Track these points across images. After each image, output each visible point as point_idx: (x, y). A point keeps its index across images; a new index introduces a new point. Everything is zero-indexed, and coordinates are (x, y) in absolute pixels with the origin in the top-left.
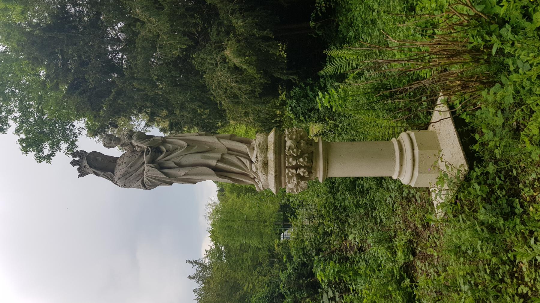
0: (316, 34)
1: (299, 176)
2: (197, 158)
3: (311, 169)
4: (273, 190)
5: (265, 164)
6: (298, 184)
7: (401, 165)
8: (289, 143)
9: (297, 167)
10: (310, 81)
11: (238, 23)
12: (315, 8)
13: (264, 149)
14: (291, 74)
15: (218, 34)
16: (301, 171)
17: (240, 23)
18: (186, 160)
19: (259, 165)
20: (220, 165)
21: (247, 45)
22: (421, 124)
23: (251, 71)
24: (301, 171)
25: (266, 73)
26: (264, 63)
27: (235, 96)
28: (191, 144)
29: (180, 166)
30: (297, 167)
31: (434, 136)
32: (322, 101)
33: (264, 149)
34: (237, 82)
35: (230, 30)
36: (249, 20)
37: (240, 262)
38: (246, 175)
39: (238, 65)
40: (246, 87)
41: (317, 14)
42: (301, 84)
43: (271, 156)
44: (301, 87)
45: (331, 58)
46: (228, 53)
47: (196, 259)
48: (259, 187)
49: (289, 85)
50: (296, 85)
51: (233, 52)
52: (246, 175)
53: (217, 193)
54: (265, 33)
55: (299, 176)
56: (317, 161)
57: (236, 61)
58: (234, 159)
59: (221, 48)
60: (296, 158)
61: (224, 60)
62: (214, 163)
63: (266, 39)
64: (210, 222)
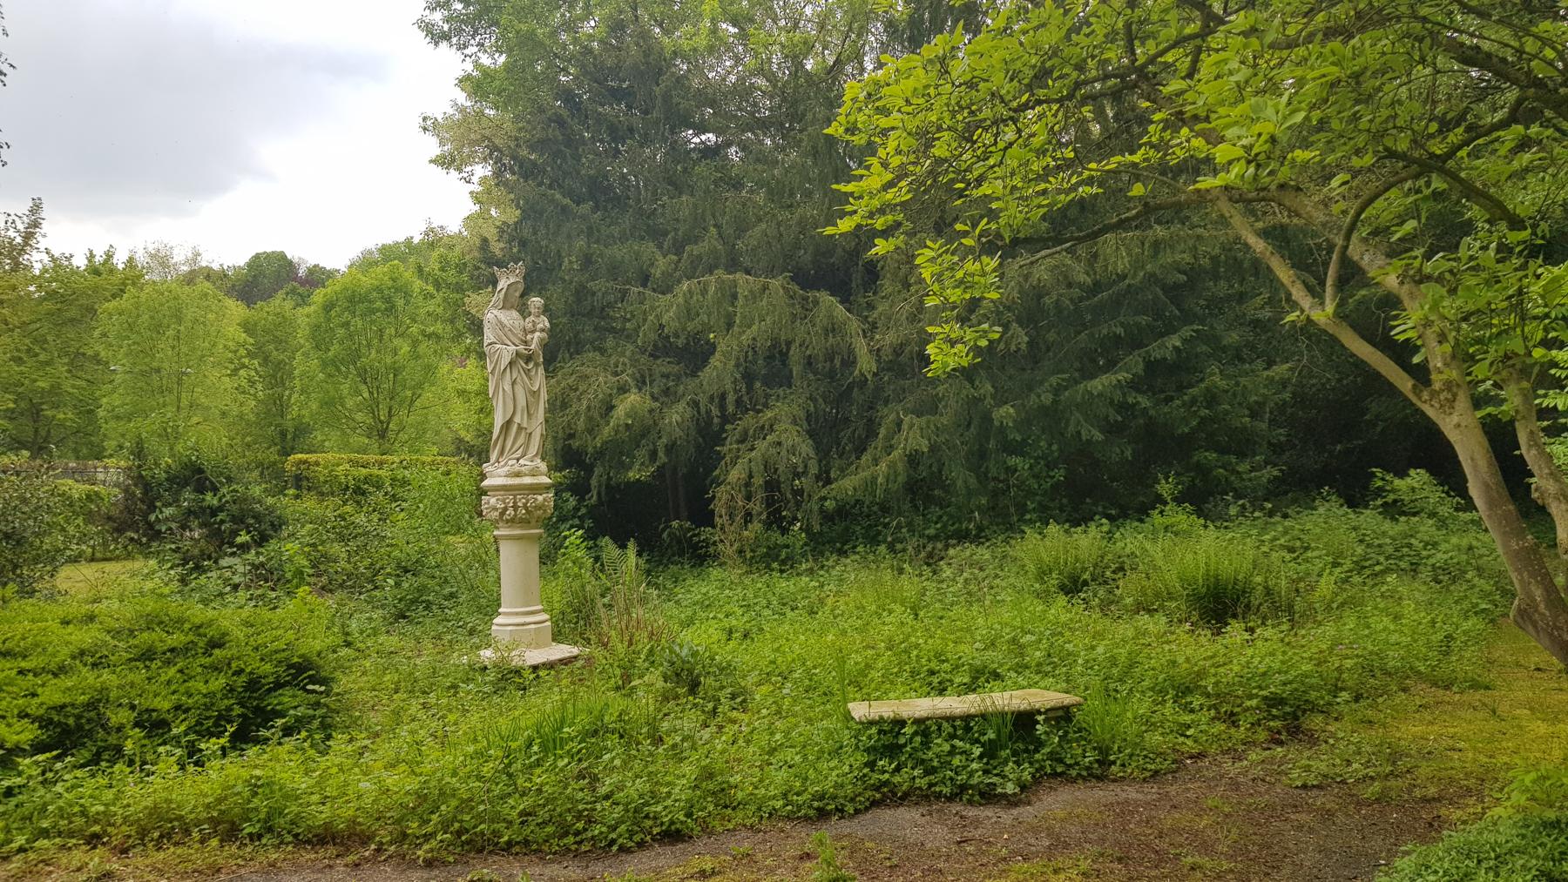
0: (663, 530)
2: (522, 402)
3: (511, 522)
4: (486, 483)
5: (518, 475)
6: (495, 509)
8: (540, 498)
9: (515, 507)
10: (588, 523)
12: (698, 526)
14: (599, 494)
15: (666, 376)
16: (510, 511)
17: (676, 418)
19: (516, 468)
20: (514, 428)
21: (641, 432)
23: (606, 432)
24: (510, 511)
25: (600, 454)
26: (616, 452)
27: (565, 405)
28: (535, 394)
29: (514, 383)
30: (515, 507)
31: (546, 645)
32: (574, 537)
36: (678, 433)
37: (42, 357)
38: (502, 453)
39: (615, 413)
40: (581, 424)
41: (689, 530)
42: (583, 511)
43: (527, 480)
44: (577, 509)
45: (623, 546)
46: (633, 398)
48: (487, 468)
50: (581, 499)
51: (633, 407)
52: (502, 453)
53: (215, 266)
55: (505, 509)
56: (522, 528)
57: (621, 411)
58: (521, 441)
59: (641, 383)
60: (525, 506)
61: (623, 390)
62: (517, 419)
63: (653, 455)
64: (142, 259)
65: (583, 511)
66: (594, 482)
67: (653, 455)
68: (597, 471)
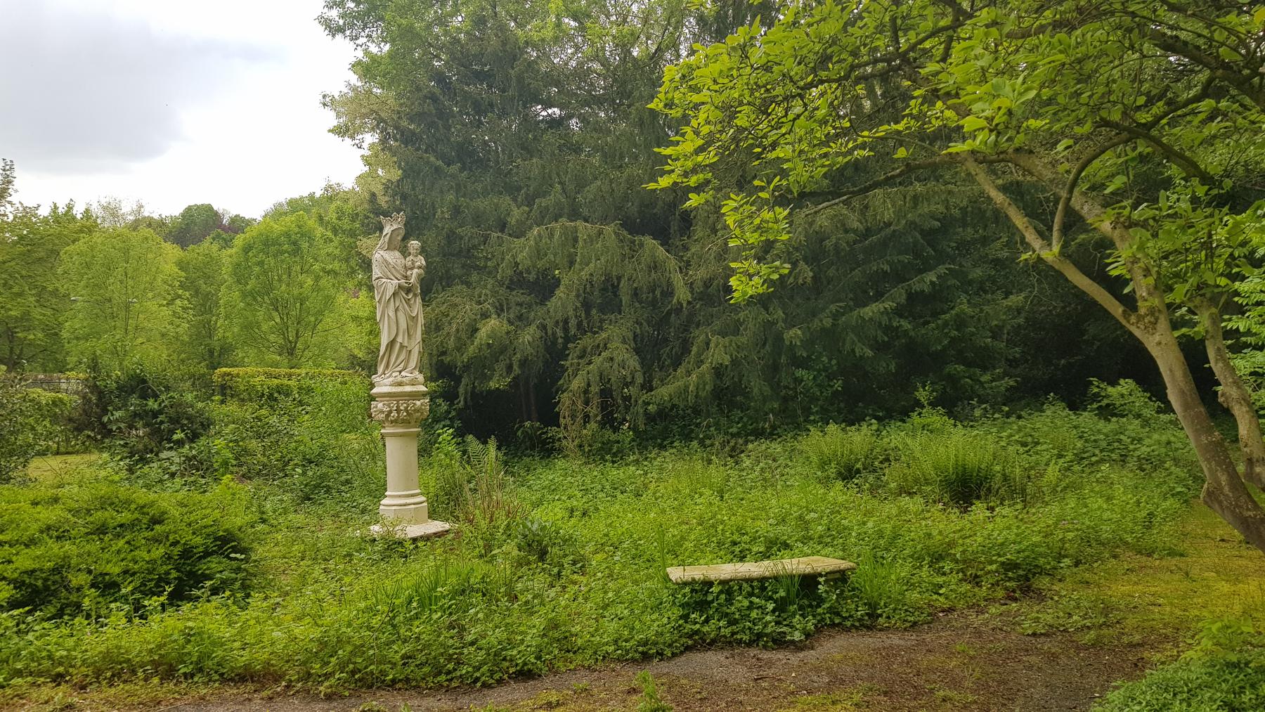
0: (518, 429)
1: (390, 412)
2: (403, 325)
3: (395, 422)
4: (374, 391)
5: (400, 384)
7: (400, 496)
8: (418, 403)
9: (398, 410)
11: (528, 336)
13: (413, 383)
14: (465, 399)
15: (520, 305)
16: (394, 414)
17: (528, 338)
18: (401, 315)
19: (399, 379)
20: (397, 346)
21: (499, 350)
22: (433, 514)
23: (472, 350)
24: (394, 414)
25: (467, 367)
26: (481, 366)
28: (414, 319)
29: (397, 310)
30: (398, 410)
33: (413, 383)
34: (458, 330)
35: (521, 320)
38: (387, 366)
39: (478, 335)
40: (451, 343)
42: (453, 413)
43: (408, 389)
44: (448, 412)
46: (493, 322)
47: (16, 182)
48: (375, 378)
49: (450, 396)
50: (450, 406)
53: (156, 216)
54: (515, 367)
55: (390, 412)
58: (402, 357)
59: (500, 310)
61: (485, 316)
62: (399, 339)
63: (510, 368)
65: (453, 413)
66: (461, 390)
67: (510, 368)
68: (464, 381)
